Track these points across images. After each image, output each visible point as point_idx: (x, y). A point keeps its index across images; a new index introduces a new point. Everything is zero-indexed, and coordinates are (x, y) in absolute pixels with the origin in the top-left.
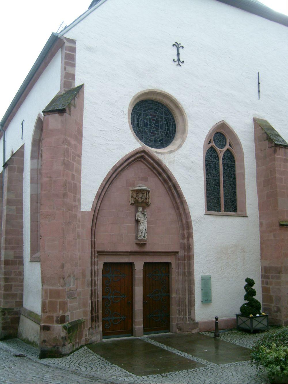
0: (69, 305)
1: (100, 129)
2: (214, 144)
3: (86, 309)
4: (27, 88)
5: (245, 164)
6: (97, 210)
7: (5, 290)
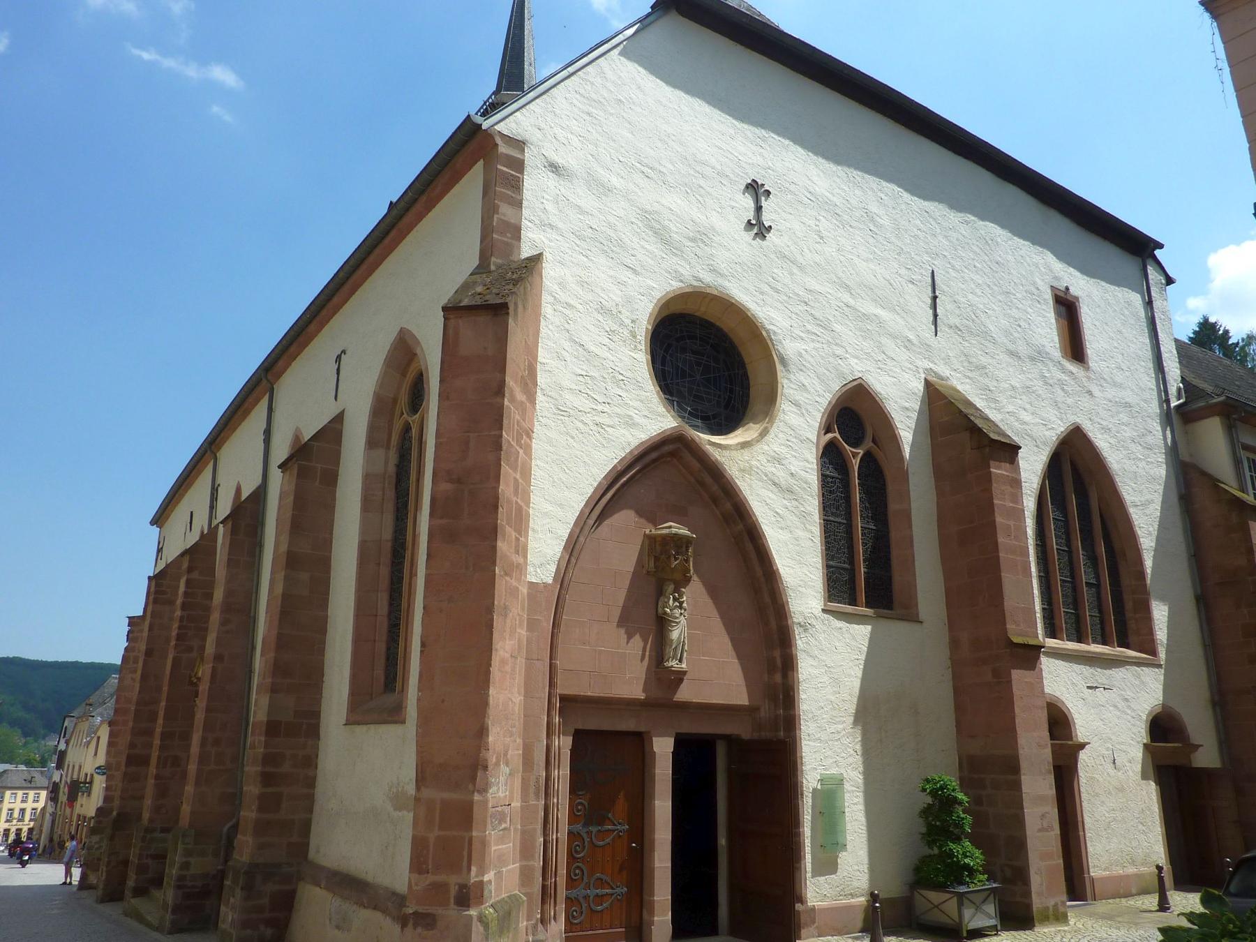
0: (493, 848)
1: (580, 372)
2: (837, 435)
3: (531, 863)
4: (364, 267)
5: (912, 487)
6: (563, 578)
7: (261, 809)
